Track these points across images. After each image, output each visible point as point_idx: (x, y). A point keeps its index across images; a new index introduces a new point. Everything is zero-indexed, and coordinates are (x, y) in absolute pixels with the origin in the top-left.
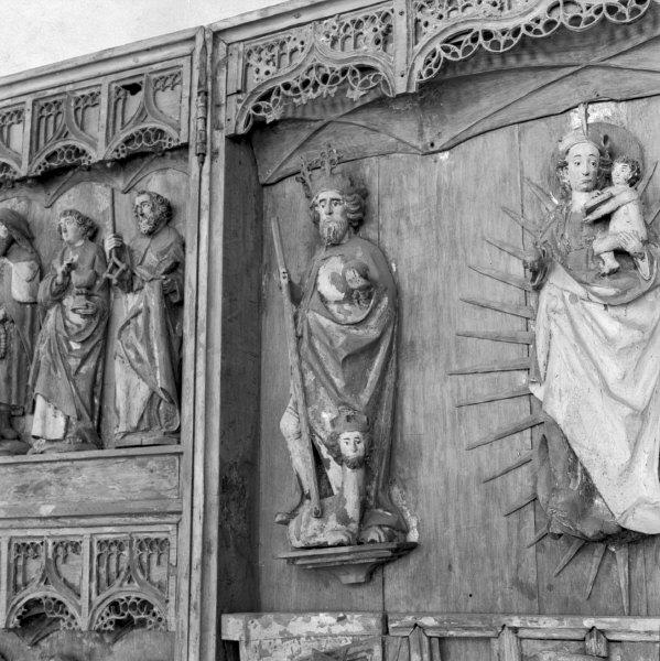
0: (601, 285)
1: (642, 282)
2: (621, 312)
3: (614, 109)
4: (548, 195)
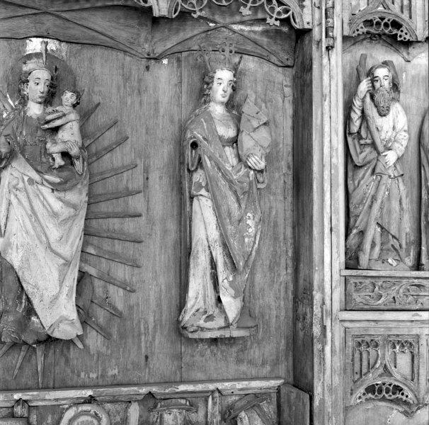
0: (52, 175)
1: (77, 176)
2: (62, 195)
3: (58, 46)
4: (6, 97)
